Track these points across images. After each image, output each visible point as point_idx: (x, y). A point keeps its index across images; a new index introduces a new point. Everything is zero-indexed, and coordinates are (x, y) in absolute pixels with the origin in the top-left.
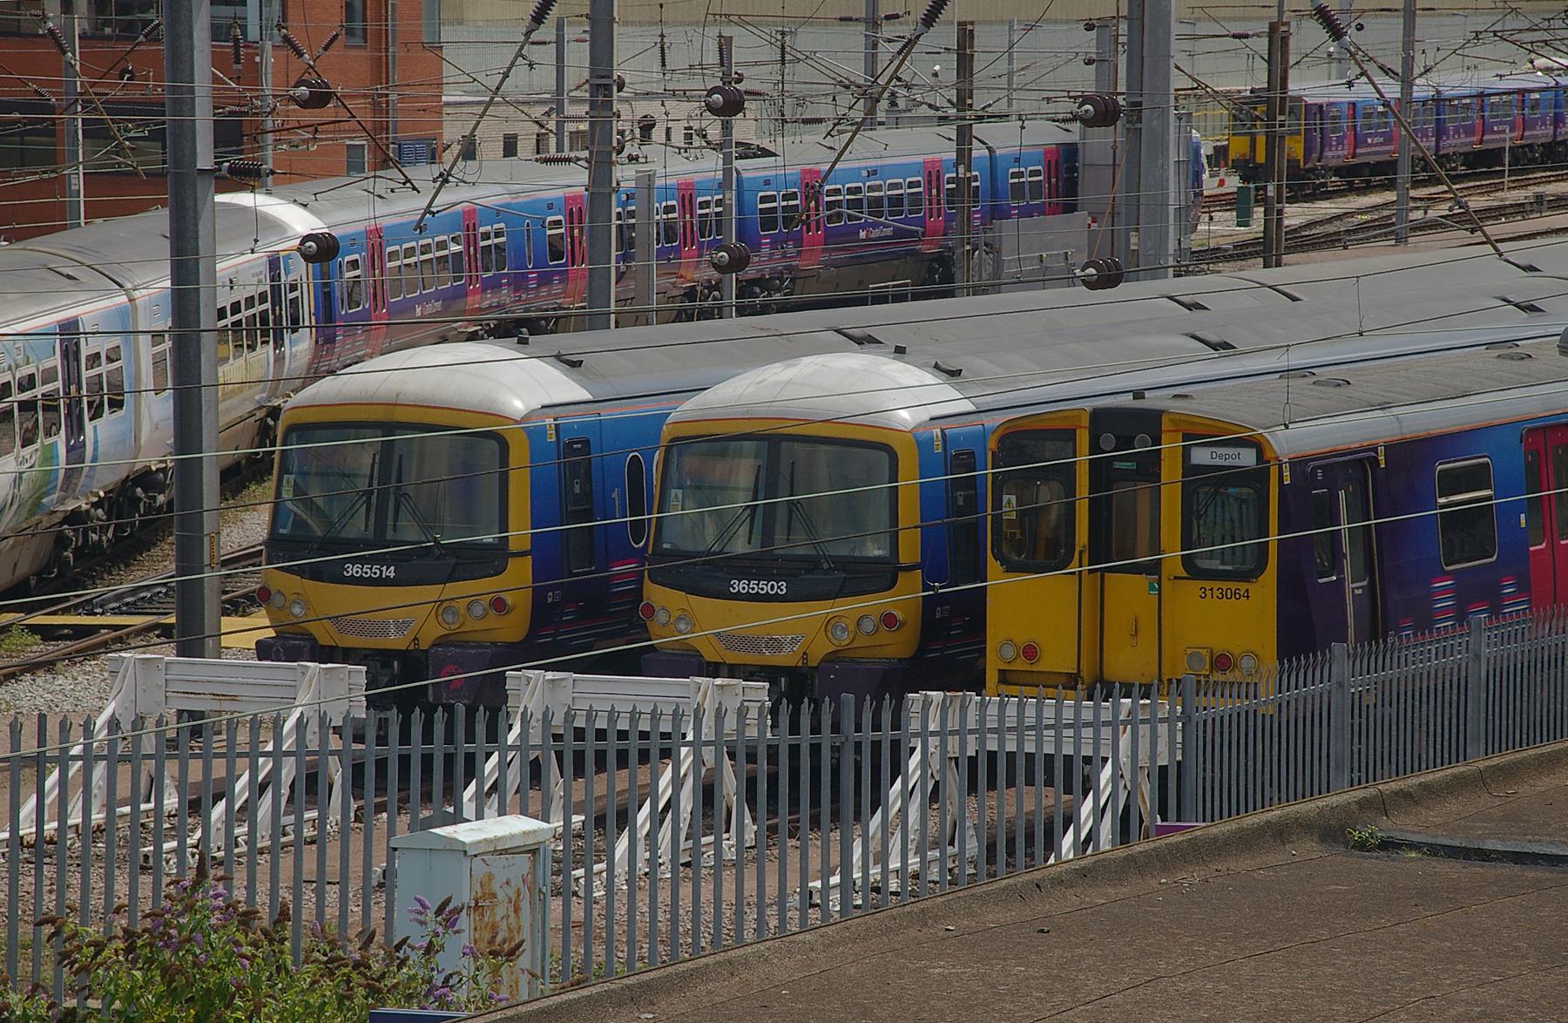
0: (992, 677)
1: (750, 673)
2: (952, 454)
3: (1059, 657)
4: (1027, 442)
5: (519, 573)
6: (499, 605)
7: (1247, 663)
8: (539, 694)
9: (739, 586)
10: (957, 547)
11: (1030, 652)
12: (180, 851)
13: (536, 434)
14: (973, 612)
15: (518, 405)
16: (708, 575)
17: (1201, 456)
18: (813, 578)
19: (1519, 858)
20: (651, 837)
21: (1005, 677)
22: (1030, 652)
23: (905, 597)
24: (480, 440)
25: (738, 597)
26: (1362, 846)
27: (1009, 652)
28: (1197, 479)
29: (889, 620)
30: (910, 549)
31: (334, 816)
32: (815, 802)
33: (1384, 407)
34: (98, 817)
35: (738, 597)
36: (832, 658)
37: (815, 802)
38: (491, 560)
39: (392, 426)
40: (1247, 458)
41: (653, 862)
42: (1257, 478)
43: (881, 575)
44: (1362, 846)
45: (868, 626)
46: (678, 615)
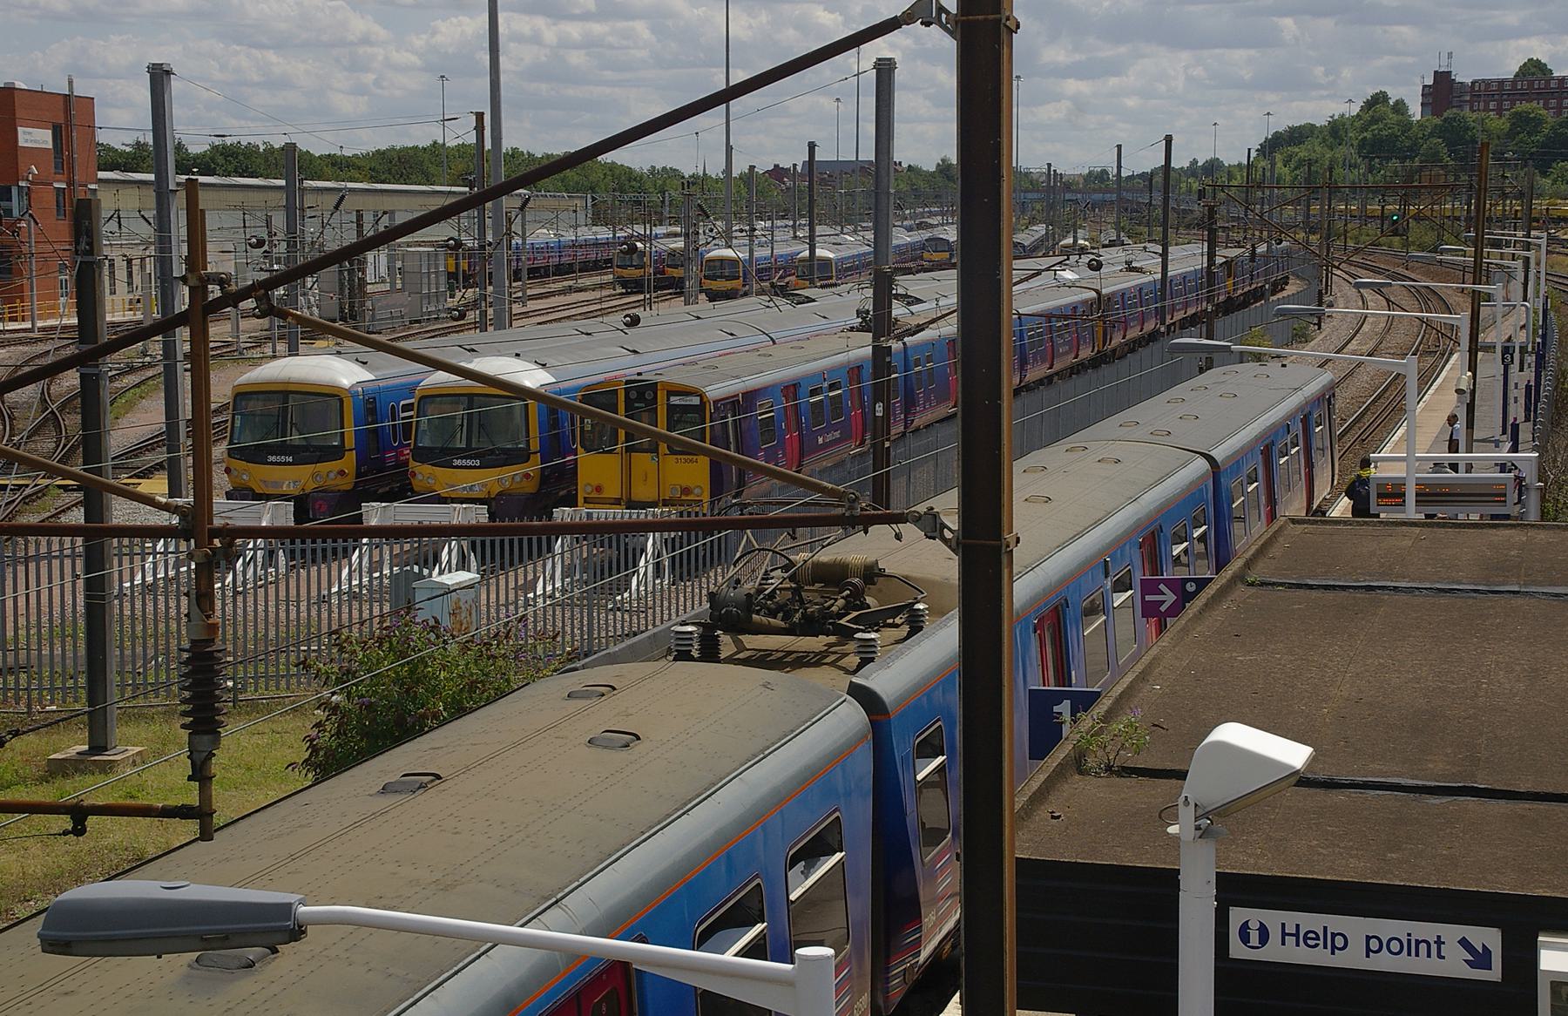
0: (580, 500)
1: (481, 501)
2: (371, 403)
3: (613, 491)
4: (599, 395)
5: (349, 462)
6: (342, 473)
7: (697, 491)
8: (375, 514)
9: (272, 458)
10: (556, 444)
11: (599, 489)
12: (223, 588)
13: (355, 395)
14: (570, 473)
15: (346, 382)
16: (441, 456)
17: (675, 400)
18: (490, 459)
19: (1326, 587)
20: (244, 573)
21: (586, 500)
22: (599, 489)
23: (533, 466)
24: (327, 397)
25: (272, 463)
26: (1252, 584)
27: (589, 489)
28: (671, 409)
29: (527, 476)
30: (535, 445)
31: (282, 570)
32: (502, 557)
33: (737, 377)
34: (171, 573)
35: (272, 463)
36: (316, 491)
37: (502, 557)
38: (337, 453)
39: (284, 395)
40: (696, 401)
41: (244, 583)
42: (700, 408)
43: (521, 456)
44: (1252, 584)
45: (518, 479)
46: (425, 474)
